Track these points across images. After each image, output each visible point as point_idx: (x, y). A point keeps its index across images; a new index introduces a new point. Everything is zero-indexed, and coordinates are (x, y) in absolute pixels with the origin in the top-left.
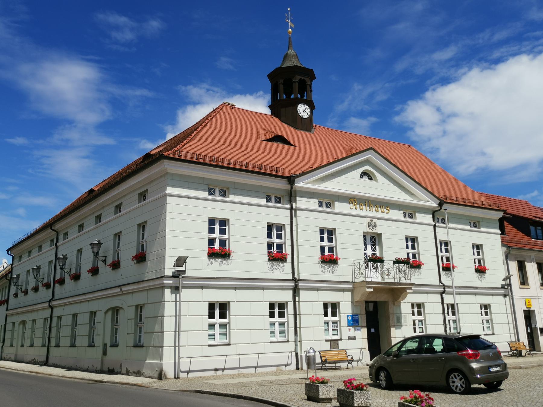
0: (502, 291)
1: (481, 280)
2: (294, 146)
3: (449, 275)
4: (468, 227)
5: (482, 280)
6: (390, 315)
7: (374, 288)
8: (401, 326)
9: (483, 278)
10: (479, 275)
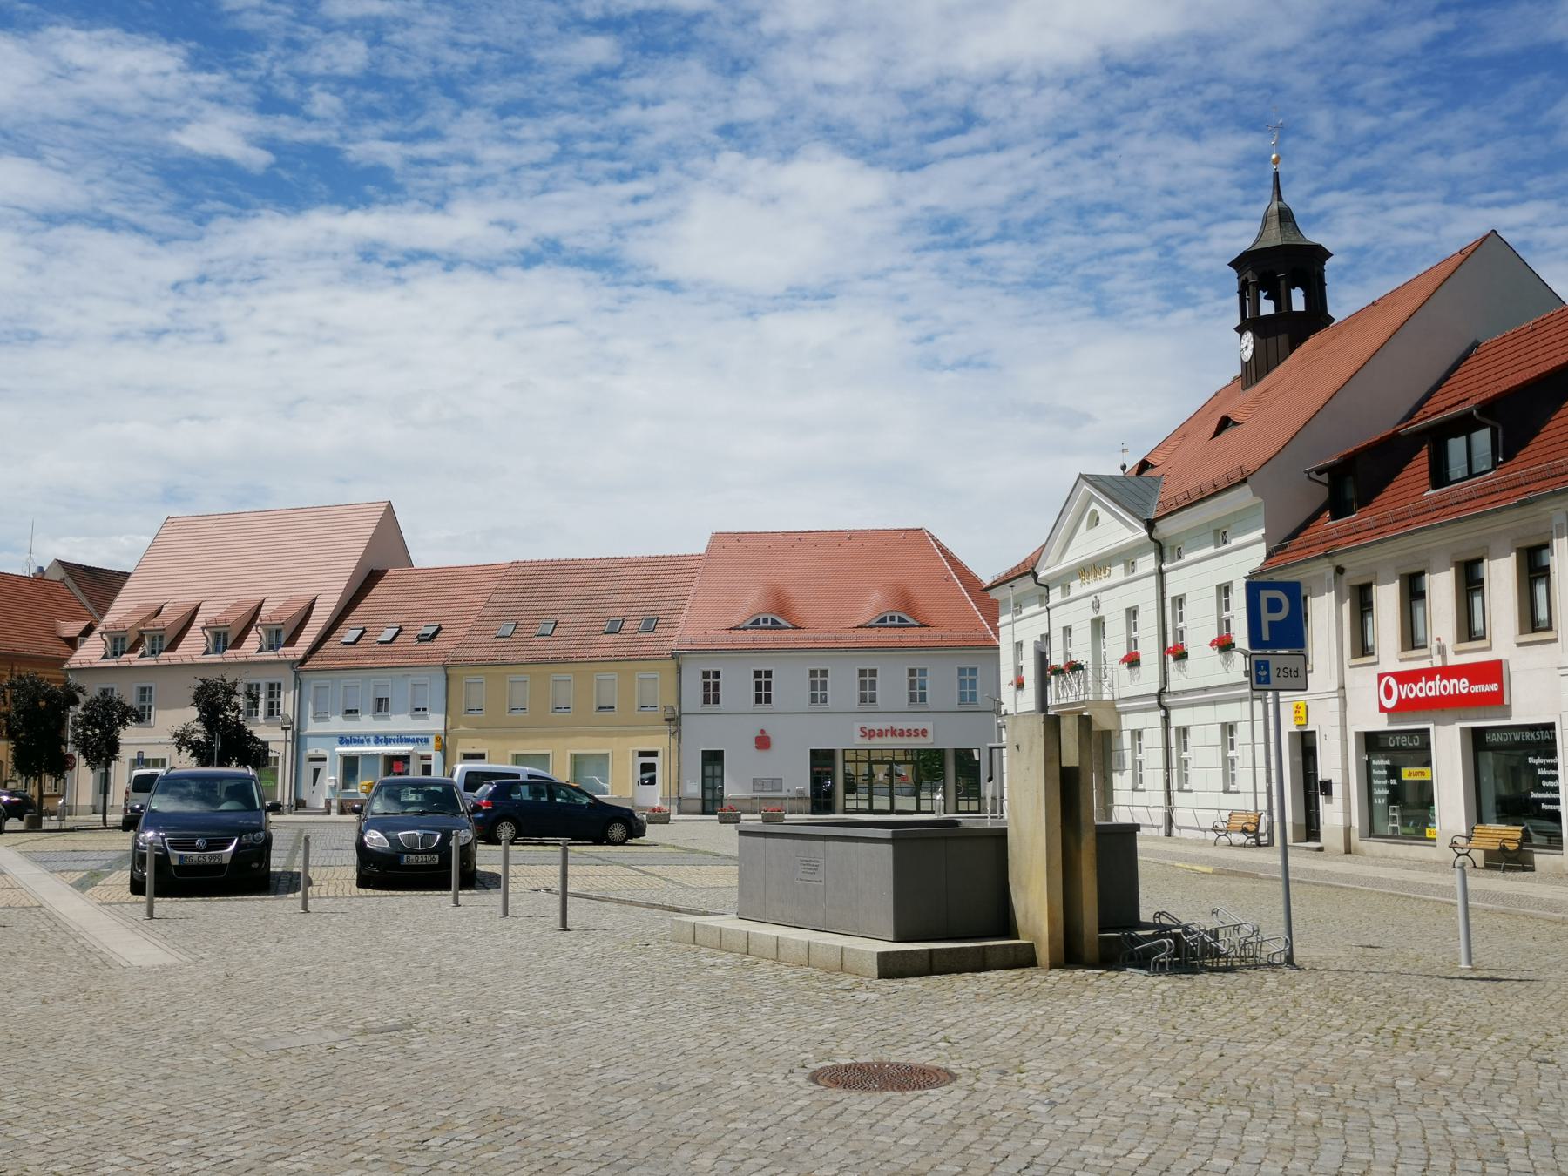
2: (1214, 437)
4: (1211, 550)
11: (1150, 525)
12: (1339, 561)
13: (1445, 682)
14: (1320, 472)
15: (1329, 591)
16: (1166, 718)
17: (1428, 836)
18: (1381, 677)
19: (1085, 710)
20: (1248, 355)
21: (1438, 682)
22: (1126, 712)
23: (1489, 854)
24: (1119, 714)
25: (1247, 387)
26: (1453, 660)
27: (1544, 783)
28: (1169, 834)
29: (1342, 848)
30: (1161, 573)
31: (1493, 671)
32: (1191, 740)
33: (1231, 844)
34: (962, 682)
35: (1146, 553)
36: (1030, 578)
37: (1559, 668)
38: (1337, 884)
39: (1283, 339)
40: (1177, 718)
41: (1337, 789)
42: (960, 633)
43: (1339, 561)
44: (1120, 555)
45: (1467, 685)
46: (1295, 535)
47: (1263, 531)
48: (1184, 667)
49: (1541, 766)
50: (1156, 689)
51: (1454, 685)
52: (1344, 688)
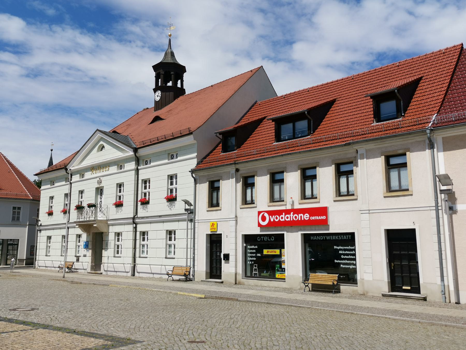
0: (41, 228)
1: (171, 208)
2: (149, 124)
3: (145, 208)
4: (166, 161)
5: (172, 209)
6: (434, 205)
7: (79, 225)
8: (108, 249)
9: (173, 206)
10: (170, 204)
11: (135, 150)
12: (238, 166)
13: (287, 216)
14: (220, 133)
15: (232, 178)
16: (136, 228)
17: (277, 277)
18: (259, 213)
19: (95, 224)
20: (158, 99)
21: (292, 215)
22: (113, 225)
23: (313, 285)
24: (109, 226)
25: (157, 110)
26: (297, 206)
27: (342, 257)
28: (134, 275)
29: (234, 283)
30: (137, 170)
31: (324, 211)
32: (52, 240)
33: (173, 280)
34: (14, 213)
35: (132, 161)
36: (64, 170)
37: (360, 211)
38: (288, 304)
39: (172, 94)
40: (140, 228)
41: (232, 258)
42: (15, 193)
43: (238, 166)
44: (78, 171)
45: (308, 216)
46: (205, 158)
47: (196, 154)
48: (146, 207)
49: (340, 250)
50: (132, 216)
51: (301, 217)
52: (163, 221)
